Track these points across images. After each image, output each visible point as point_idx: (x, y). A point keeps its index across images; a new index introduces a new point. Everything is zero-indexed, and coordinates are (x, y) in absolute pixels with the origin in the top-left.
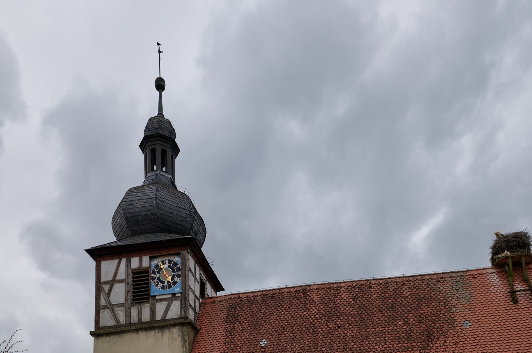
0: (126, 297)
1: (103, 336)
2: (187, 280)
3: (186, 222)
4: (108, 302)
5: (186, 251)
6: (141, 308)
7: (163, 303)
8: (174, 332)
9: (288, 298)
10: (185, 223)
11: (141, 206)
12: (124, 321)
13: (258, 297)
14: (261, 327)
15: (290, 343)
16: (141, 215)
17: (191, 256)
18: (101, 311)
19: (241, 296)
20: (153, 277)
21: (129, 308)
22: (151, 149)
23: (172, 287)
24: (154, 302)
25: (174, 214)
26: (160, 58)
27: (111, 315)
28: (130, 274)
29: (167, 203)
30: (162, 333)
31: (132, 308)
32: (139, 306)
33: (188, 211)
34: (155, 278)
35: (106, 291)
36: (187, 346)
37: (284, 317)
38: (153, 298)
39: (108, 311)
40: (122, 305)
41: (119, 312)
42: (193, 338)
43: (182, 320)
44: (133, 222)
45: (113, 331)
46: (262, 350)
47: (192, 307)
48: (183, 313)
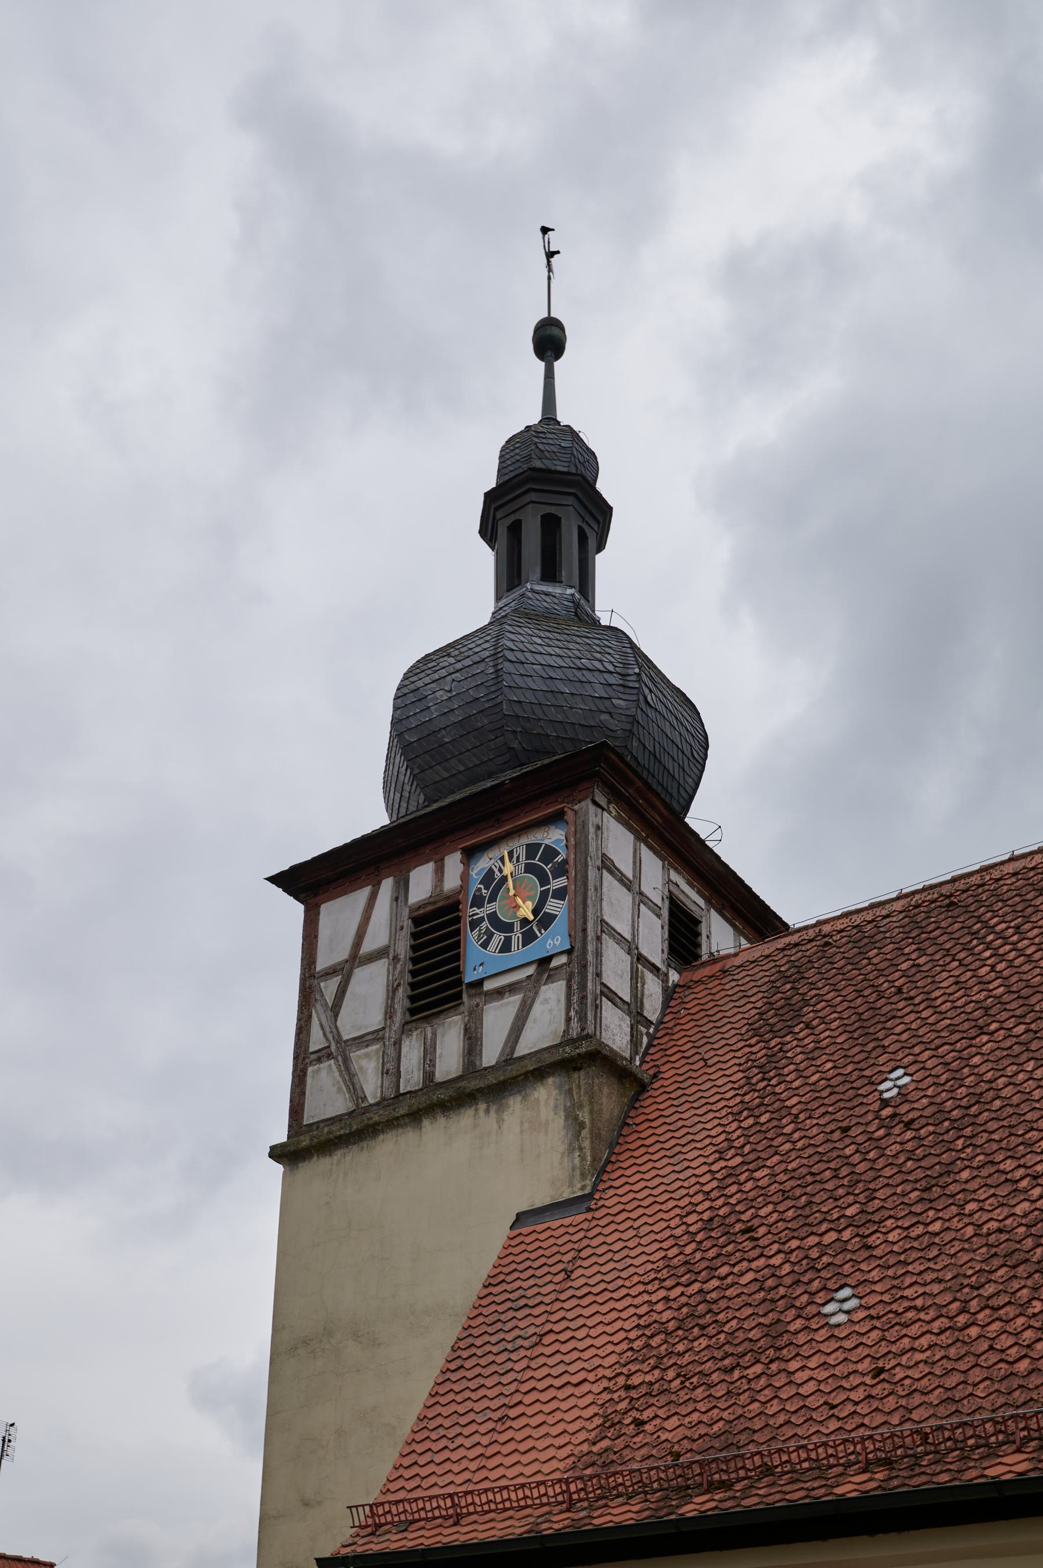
0: (387, 1007)
1: (311, 1156)
2: (589, 901)
3: (610, 713)
4: (333, 1038)
5: (589, 801)
6: (434, 1034)
7: (505, 1001)
8: (541, 1099)
9: (1017, 895)
10: (604, 717)
11: (449, 695)
12: (377, 1093)
13: (894, 919)
14: (889, 1024)
15: (1012, 1064)
16: (448, 726)
17: (615, 818)
18: (310, 1069)
19: (827, 929)
20: (475, 917)
21: (395, 1043)
22: (542, 516)
23: (537, 937)
24: (477, 1005)
25: (562, 693)
26: (550, 270)
27: (339, 1079)
28: (405, 924)
29: (533, 664)
30: (500, 1110)
31: (403, 1042)
32: (429, 1030)
33: (618, 673)
34: (482, 919)
35: (328, 1001)
36: (587, 1144)
37: (993, 967)
38: (473, 991)
39: (330, 1066)
40: (376, 1036)
41: (364, 1063)
42: (616, 1112)
43: (567, 1049)
44: (427, 757)
45: (338, 1133)
46: (887, 1112)
47: (621, 999)
48: (575, 1024)
